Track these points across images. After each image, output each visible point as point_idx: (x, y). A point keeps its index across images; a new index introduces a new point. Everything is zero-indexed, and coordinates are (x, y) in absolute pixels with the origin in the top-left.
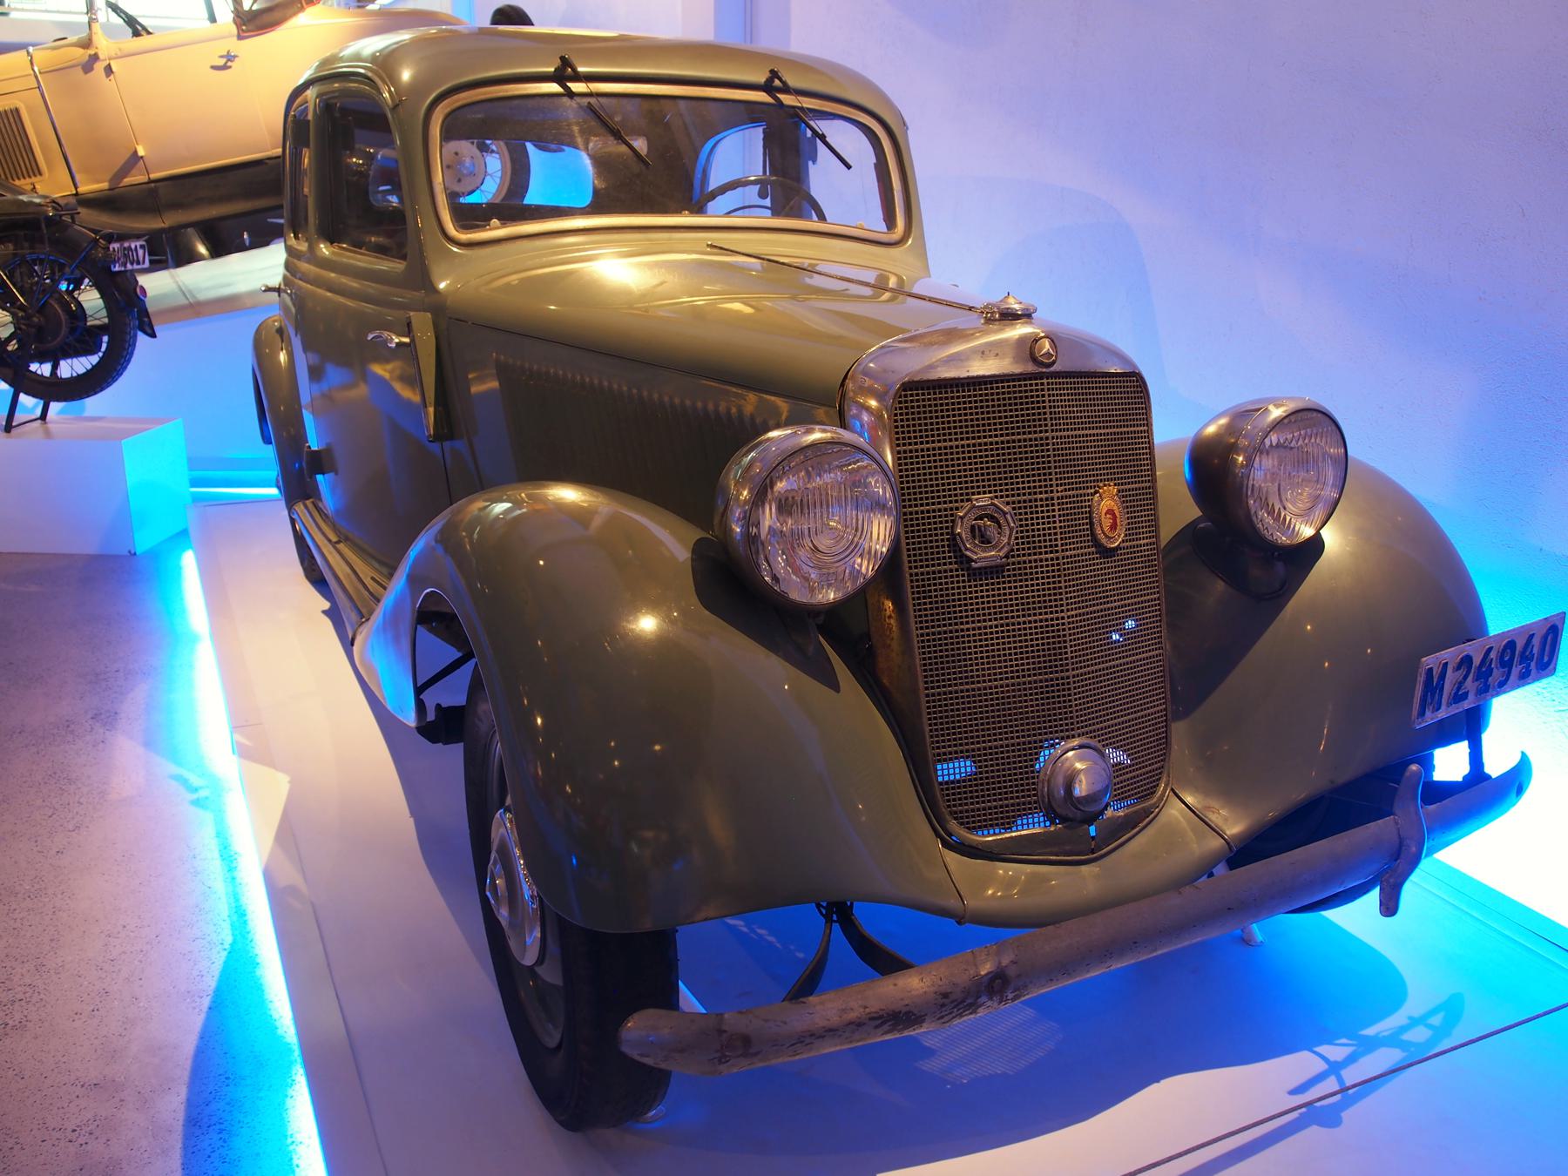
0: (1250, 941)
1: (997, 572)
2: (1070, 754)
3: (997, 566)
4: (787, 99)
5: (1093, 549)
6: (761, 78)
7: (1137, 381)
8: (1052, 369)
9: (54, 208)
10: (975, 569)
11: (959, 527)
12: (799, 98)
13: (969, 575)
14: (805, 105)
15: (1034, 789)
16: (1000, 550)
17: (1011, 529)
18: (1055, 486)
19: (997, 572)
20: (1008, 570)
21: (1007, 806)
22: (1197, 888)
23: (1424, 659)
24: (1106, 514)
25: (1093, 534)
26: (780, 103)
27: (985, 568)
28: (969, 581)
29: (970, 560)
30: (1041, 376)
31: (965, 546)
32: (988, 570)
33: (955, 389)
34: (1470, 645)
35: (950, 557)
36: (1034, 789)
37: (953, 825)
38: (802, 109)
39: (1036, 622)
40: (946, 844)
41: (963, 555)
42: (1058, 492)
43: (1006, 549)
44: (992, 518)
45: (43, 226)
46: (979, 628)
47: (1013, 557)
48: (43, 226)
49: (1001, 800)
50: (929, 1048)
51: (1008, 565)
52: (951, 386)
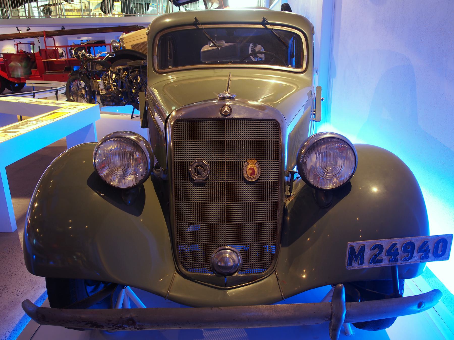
0: (347, 333)
1: (203, 185)
2: (229, 251)
3: (203, 183)
4: (200, 27)
5: (243, 181)
6: (261, 21)
7: (275, 123)
8: (229, 117)
9: (144, 63)
10: (195, 183)
11: (190, 168)
12: (202, 27)
13: (193, 185)
14: (273, 28)
15: (209, 260)
16: (203, 178)
17: (208, 171)
18: (225, 158)
19: (203, 185)
20: (207, 185)
21: (200, 264)
22: (220, 309)
23: (349, 243)
24: (249, 169)
25: (243, 176)
26: (266, 28)
27: (197, 183)
28: (193, 187)
29: (194, 180)
30: (224, 119)
31: (192, 175)
32: (200, 184)
33: (192, 122)
34: (381, 241)
35: (188, 178)
36: (209, 260)
37: (181, 266)
38: (272, 29)
39: (237, 203)
40: (177, 271)
41: (192, 178)
42: (227, 160)
43: (205, 177)
44: (201, 166)
45: (141, 68)
46: (247, 203)
47: (260, 180)
48: (141, 68)
49: (247, 262)
50: (204, 336)
51: (207, 183)
52: (203, 121)
